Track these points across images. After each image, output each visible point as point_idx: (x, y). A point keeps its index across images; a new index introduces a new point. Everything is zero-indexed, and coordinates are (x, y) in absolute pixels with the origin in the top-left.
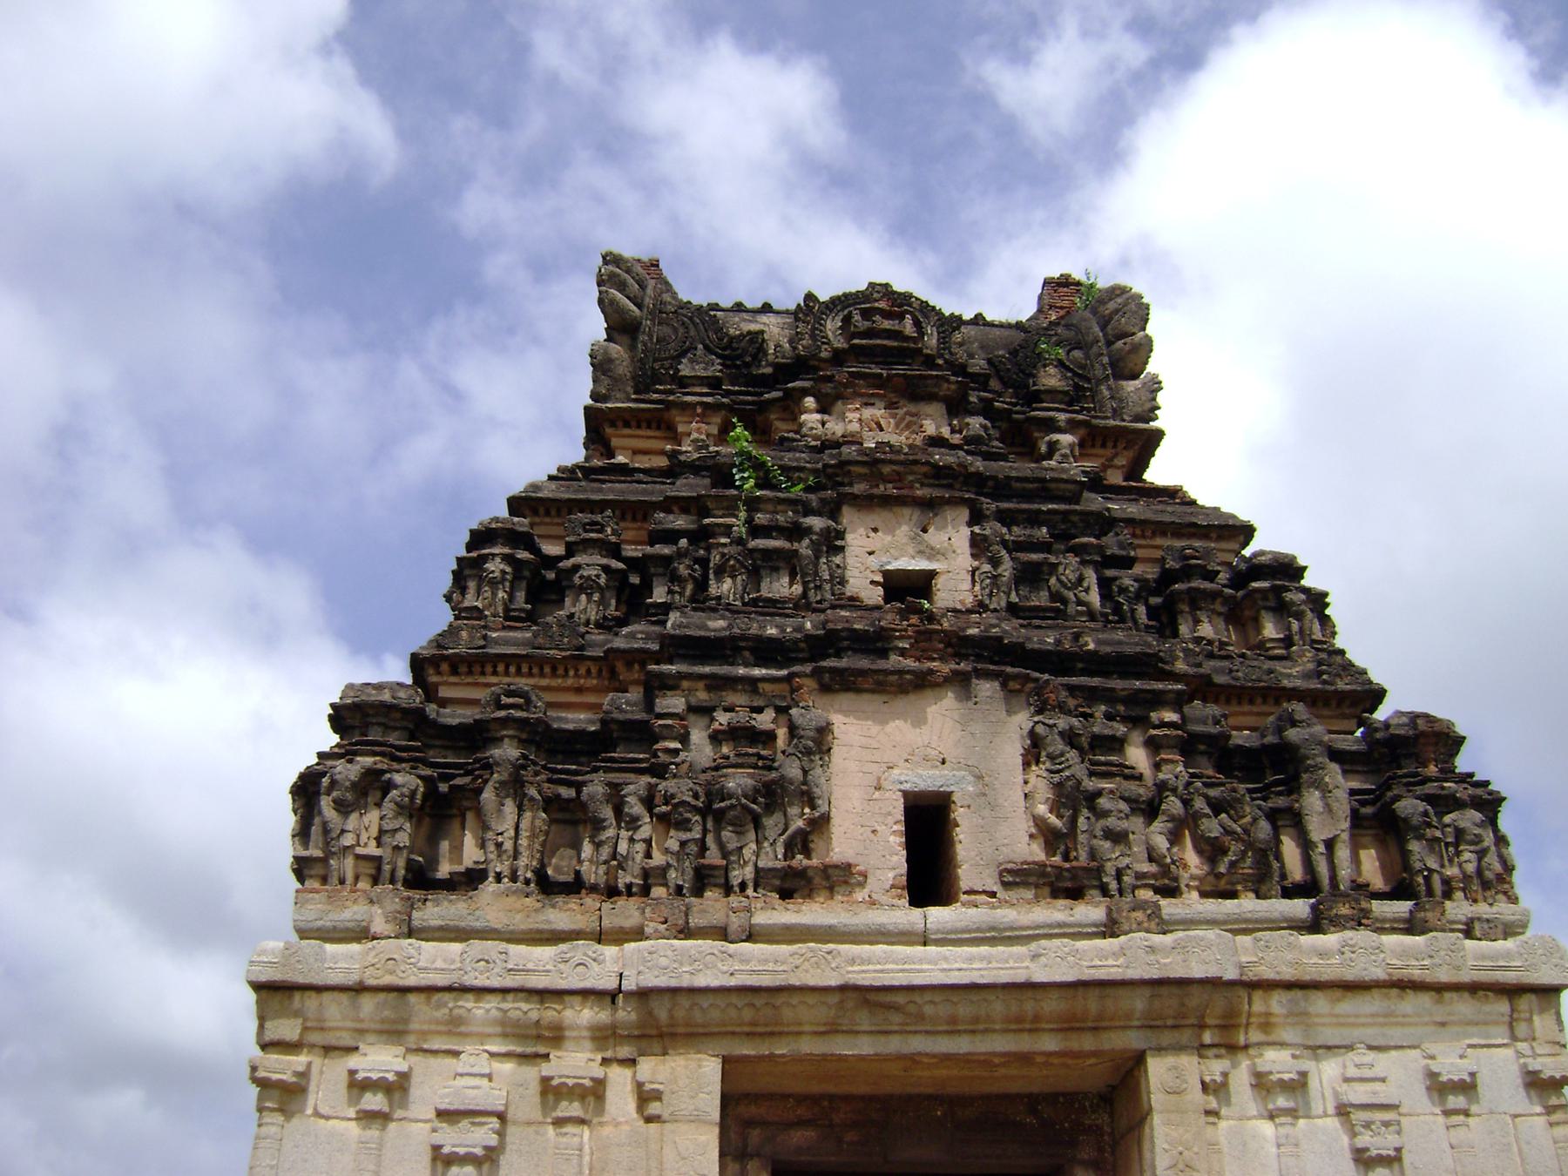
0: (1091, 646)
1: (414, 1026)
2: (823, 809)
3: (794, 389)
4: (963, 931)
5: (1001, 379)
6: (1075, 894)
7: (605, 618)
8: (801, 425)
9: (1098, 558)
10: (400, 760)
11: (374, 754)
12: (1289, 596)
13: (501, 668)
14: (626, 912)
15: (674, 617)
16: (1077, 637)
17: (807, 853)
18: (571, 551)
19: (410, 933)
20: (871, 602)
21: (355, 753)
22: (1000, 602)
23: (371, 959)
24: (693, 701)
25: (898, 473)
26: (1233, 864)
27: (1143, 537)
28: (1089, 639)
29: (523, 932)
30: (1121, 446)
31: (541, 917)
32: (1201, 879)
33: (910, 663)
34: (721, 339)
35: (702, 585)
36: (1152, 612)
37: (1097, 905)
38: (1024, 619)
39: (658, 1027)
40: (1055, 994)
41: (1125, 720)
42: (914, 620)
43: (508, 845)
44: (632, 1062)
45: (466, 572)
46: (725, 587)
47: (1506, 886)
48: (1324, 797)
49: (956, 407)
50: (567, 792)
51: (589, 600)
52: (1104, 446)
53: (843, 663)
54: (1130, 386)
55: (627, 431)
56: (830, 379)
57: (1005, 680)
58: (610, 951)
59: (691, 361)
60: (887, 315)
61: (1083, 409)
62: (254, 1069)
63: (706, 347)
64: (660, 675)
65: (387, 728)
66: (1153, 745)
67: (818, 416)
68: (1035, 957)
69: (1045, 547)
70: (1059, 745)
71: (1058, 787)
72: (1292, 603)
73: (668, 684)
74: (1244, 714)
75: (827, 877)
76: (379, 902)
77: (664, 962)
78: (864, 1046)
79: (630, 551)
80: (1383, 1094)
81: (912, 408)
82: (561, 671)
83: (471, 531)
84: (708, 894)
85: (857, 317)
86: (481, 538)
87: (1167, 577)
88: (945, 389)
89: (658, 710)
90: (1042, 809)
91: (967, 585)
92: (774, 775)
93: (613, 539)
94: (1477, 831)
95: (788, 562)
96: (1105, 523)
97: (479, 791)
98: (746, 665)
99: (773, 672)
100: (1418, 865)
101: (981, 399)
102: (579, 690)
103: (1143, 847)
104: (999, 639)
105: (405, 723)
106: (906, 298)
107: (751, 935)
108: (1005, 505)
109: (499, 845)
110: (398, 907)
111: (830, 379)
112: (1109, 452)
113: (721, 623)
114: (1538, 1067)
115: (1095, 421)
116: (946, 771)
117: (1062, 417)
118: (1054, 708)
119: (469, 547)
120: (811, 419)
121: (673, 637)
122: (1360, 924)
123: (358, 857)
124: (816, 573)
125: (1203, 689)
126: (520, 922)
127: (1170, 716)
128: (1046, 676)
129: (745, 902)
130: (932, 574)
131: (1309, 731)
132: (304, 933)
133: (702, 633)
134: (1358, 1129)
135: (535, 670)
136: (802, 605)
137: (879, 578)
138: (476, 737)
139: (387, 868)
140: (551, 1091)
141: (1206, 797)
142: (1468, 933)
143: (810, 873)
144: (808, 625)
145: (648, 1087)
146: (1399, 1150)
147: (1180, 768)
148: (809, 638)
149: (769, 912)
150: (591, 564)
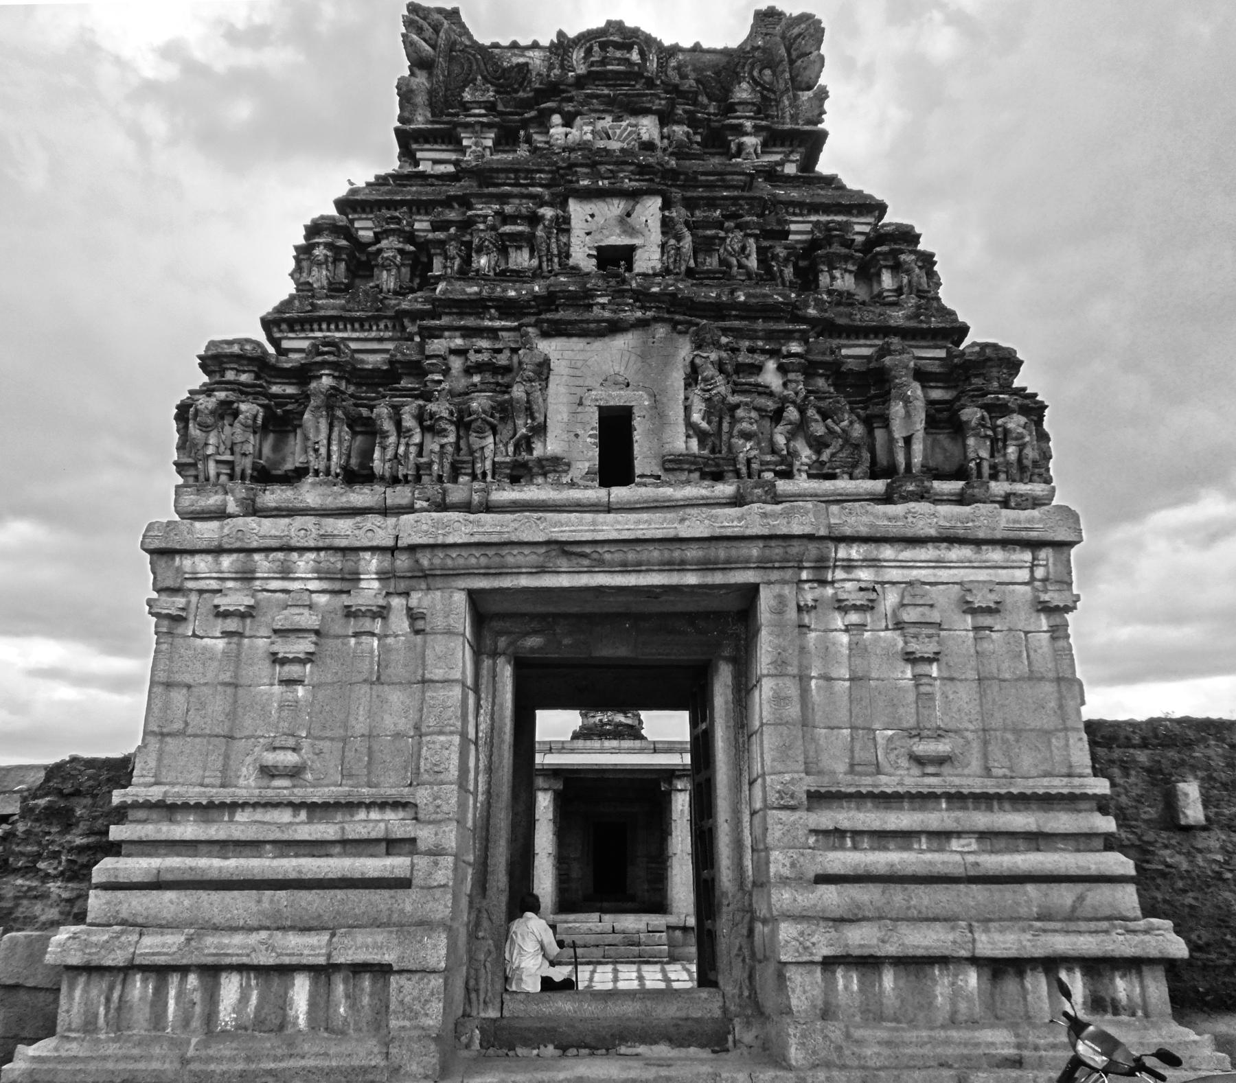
0: (742, 298)
3: (544, 109)
4: (636, 503)
6: (718, 477)
8: (551, 137)
9: (758, 232)
10: (247, 394)
11: (227, 390)
12: (903, 257)
13: (324, 326)
14: (399, 495)
15: (441, 286)
16: (732, 292)
17: (530, 450)
20: (587, 270)
21: (214, 390)
23: (226, 531)
24: (452, 346)
25: (611, 171)
26: (833, 455)
27: (801, 215)
30: (796, 143)
31: (344, 499)
32: (810, 466)
33: (607, 314)
35: (467, 261)
36: (798, 271)
39: (422, 570)
43: (323, 451)
44: (406, 594)
45: (304, 253)
47: (1043, 470)
48: (906, 406)
49: (665, 119)
50: (365, 412)
51: (389, 275)
52: (782, 145)
53: (561, 315)
54: (805, 96)
57: (674, 324)
58: (391, 521)
60: (618, 46)
63: (484, 78)
66: (782, 369)
68: (682, 520)
70: (710, 371)
72: (906, 262)
74: (860, 346)
75: (542, 467)
76: (232, 492)
77: (425, 527)
78: (564, 581)
81: (633, 120)
82: (367, 327)
84: (461, 479)
85: (596, 48)
86: (314, 230)
87: (813, 245)
88: (659, 104)
89: (427, 353)
91: (657, 255)
93: (407, 229)
94: (1020, 430)
95: (529, 241)
96: (765, 206)
97: (302, 414)
98: (491, 319)
99: (508, 324)
100: (972, 455)
101: (685, 111)
102: (381, 340)
105: (251, 368)
106: (636, 32)
107: (488, 508)
109: (316, 451)
110: (244, 495)
111: (571, 100)
113: (476, 289)
115: (776, 126)
117: (748, 124)
118: (708, 344)
119: (307, 238)
120: (557, 131)
121: (440, 300)
123: (218, 462)
124: (548, 249)
125: (828, 328)
126: (330, 502)
127: (795, 348)
128: (705, 321)
129: (483, 485)
130: (632, 249)
135: (349, 326)
136: (537, 274)
139: (238, 470)
143: (531, 464)
144: (537, 288)
145: (415, 611)
148: (536, 297)
150: (390, 245)
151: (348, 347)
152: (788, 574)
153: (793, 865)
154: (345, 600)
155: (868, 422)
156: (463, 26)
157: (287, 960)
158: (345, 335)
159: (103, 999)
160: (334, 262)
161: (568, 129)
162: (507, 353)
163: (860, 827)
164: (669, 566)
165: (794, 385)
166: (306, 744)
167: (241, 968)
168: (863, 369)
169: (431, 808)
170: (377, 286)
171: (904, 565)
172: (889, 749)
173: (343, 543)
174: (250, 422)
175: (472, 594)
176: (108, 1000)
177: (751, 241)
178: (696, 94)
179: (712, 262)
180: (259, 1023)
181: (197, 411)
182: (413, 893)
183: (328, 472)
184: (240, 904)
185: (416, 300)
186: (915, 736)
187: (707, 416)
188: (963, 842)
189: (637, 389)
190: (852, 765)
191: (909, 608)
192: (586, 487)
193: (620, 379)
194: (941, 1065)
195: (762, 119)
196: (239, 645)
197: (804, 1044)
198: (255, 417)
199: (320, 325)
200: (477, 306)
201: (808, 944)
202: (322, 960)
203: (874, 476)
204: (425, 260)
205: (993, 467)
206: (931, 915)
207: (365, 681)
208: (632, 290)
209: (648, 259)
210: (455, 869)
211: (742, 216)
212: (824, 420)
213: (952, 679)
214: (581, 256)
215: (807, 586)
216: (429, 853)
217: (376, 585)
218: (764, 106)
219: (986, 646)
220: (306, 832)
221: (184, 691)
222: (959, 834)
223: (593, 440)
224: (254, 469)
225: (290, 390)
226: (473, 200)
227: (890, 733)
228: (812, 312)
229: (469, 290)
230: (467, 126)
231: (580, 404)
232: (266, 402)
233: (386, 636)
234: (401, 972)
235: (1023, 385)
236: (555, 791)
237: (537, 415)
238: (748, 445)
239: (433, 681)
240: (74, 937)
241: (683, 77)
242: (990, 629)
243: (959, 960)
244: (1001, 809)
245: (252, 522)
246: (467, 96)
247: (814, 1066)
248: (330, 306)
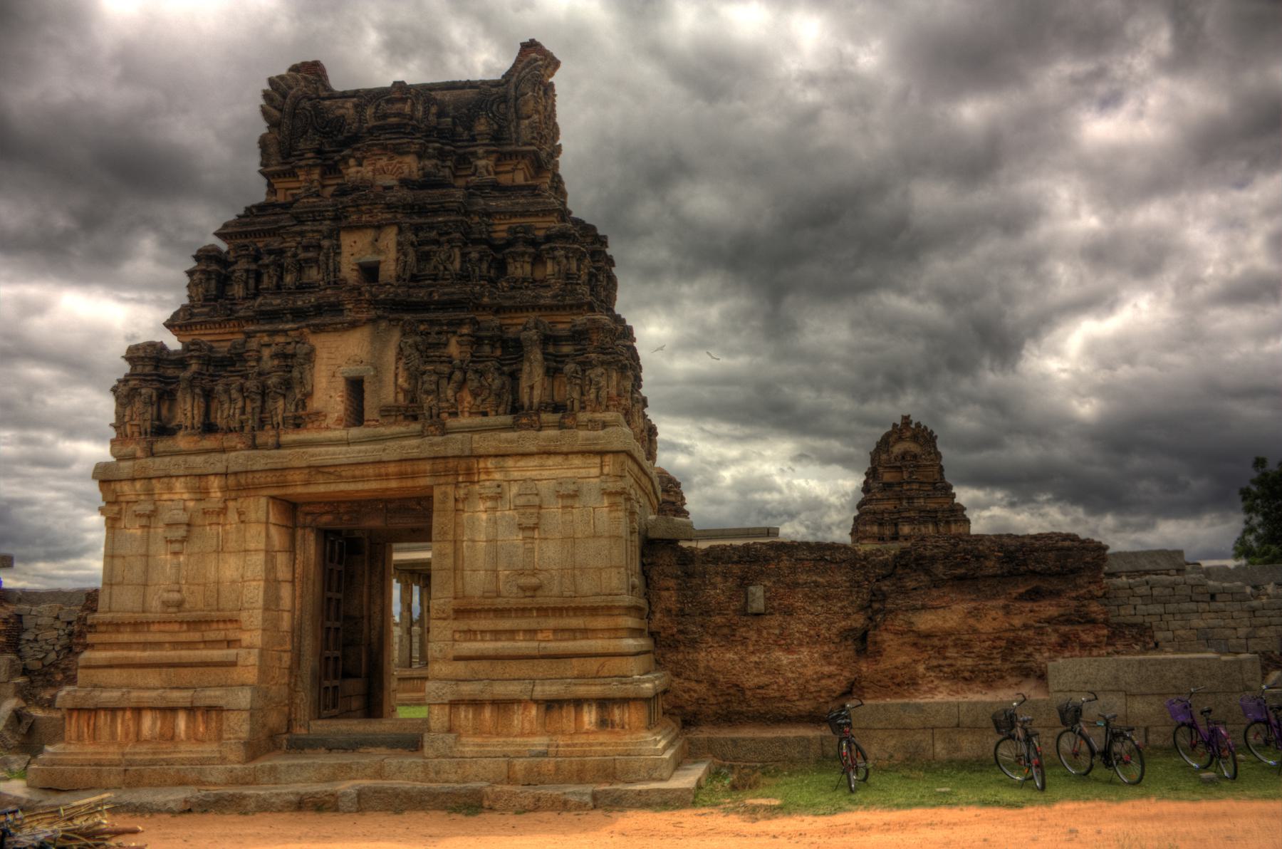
0: (436, 298)
1: (156, 491)
2: (309, 388)
17: (304, 407)
24: (262, 342)
30: (520, 158)
40: (393, 465)
43: (189, 414)
58: (225, 456)
78: (322, 489)
81: (400, 159)
85: (383, 104)
102: (232, 333)
111: (358, 149)
112: (515, 162)
117: (480, 151)
126: (192, 446)
130: (379, 262)
137: (355, 267)
144: (313, 300)
152: (450, 479)
153: (441, 651)
154: (203, 505)
161: (359, 168)
162: (293, 344)
163: (485, 628)
164: (379, 477)
166: (184, 588)
167: (152, 709)
169: (248, 623)
171: (521, 469)
173: (199, 472)
176: (88, 725)
179: (429, 269)
180: (162, 736)
182: (239, 669)
183: (193, 428)
184: (153, 678)
188: (544, 635)
192: (335, 429)
193: (357, 358)
196: (148, 532)
198: (151, 397)
202: (188, 705)
205: (582, 402)
209: (389, 269)
211: (450, 233)
213: (546, 539)
214: (348, 271)
215: (463, 485)
217: (219, 494)
220: (183, 637)
221: (121, 560)
222: (541, 631)
224: (152, 427)
227: (507, 572)
230: (300, 167)
231: (334, 376)
234: (228, 710)
238: (430, 398)
240: (68, 693)
242: (572, 507)
243: (526, 702)
244: (568, 616)
245: (150, 461)
246: (302, 146)
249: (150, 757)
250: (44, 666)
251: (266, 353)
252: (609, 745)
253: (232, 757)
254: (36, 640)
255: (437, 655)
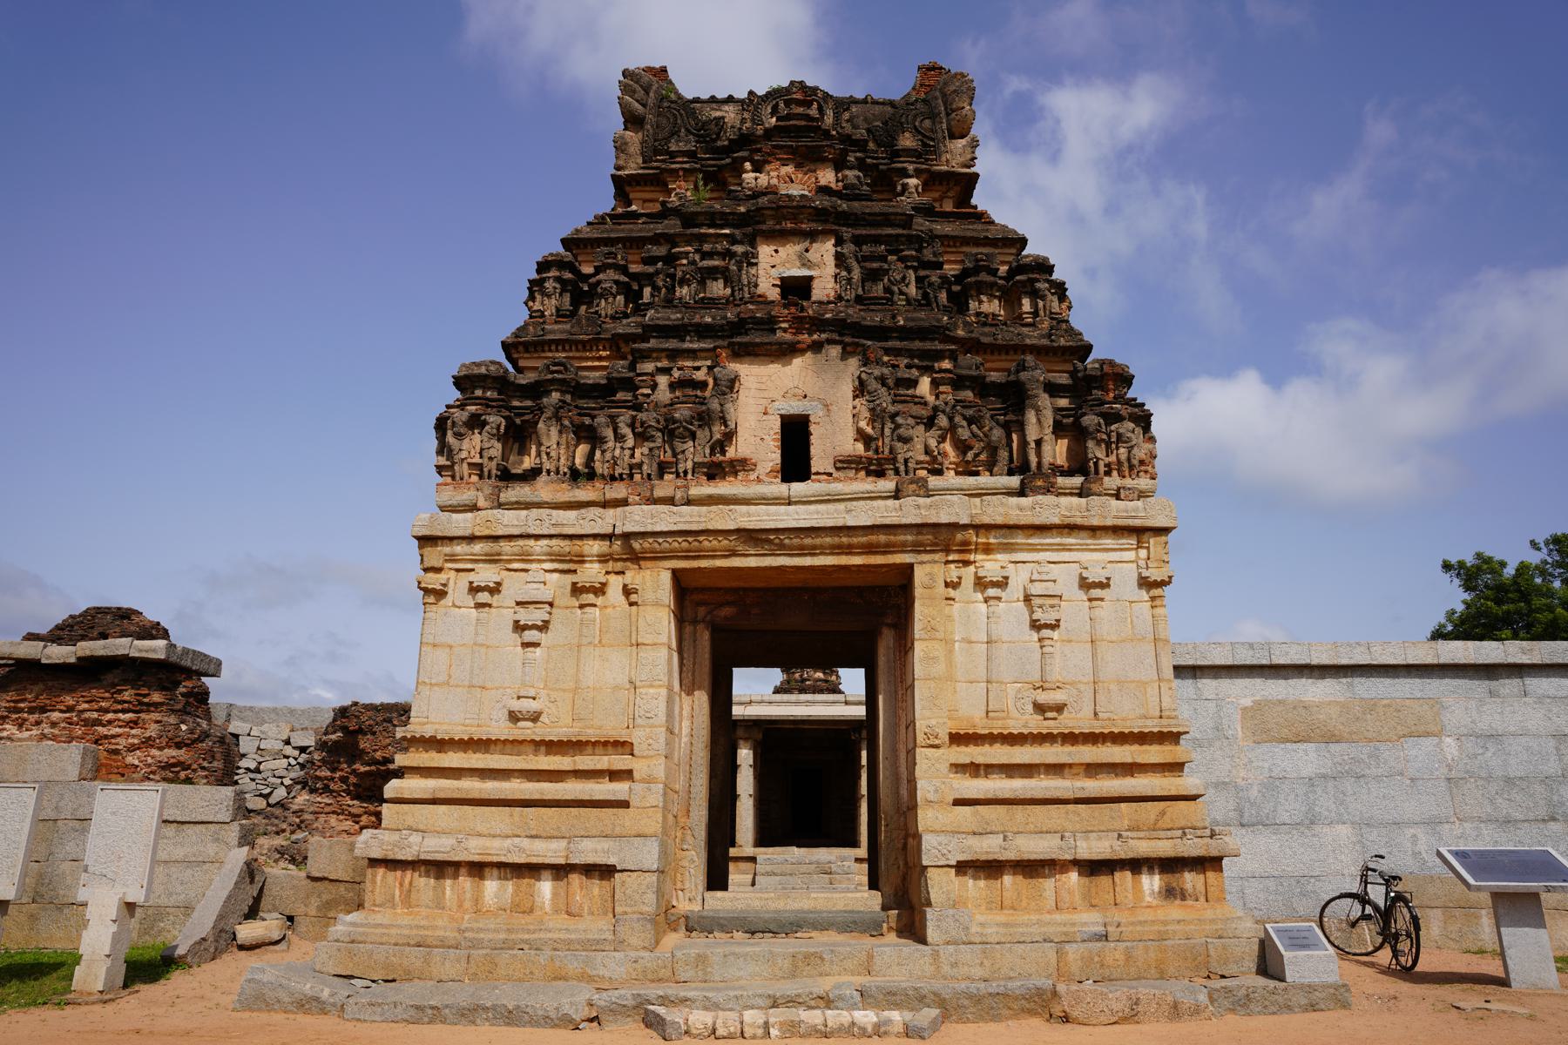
0: (902, 323)
5: (875, 141)
6: (880, 474)
7: (616, 313)
8: (743, 181)
9: (916, 264)
10: (493, 407)
11: (476, 405)
12: (1038, 285)
13: (553, 348)
14: (618, 491)
15: (651, 313)
16: (894, 317)
17: (723, 452)
18: (598, 270)
19: (500, 506)
21: (466, 405)
22: (850, 295)
24: (659, 365)
26: (977, 455)
27: (955, 246)
28: (900, 318)
29: (562, 503)
30: (952, 184)
33: (788, 337)
34: (697, 124)
35: (672, 290)
36: (950, 295)
37: (892, 480)
38: (865, 305)
41: (918, 368)
42: (793, 310)
45: (536, 287)
46: (683, 292)
49: (839, 165)
50: (587, 421)
52: (941, 184)
55: (638, 188)
56: (759, 150)
58: (611, 512)
59: (677, 141)
60: (799, 103)
61: (927, 160)
62: (419, 583)
63: (687, 130)
64: (639, 350)
65: (485, 389)
66: (935, 384)
67: (753, 175)
69: (884, 259)
70: (873, 385)
71: (872, 410)
72: (1040, 290)
73: (646, 355)
74: (1001, 361)
77: (637, 518)
78: (752, 562)
79: (635, 268)
80: (1051, 589)
82: (588, 348)
83: (537, 263)
84: (666, 477)
85: (782, 105)
86: (543, 266)
87: (965, 273)
90: (863, 424)
92: (704, 408)
96: (918, 241)
97: (537, 423)
100: (1090, 456)
101: (856, 158)
102: (600, 358)
103: (923, 446)
104: (844, 320)
105: (495, 385)
106: (815, 89)
108: (858, 232)
111: (759, 150)
112: (944, 188)
114: (1147, 575)
116: (806, 402)
117: (911, 167)
119: (539, 271)
120: (749, 177)
121: (649, 326)
122: (1049, 491)
123: (469, 464)
124: (740, 281)
125: (973, 346)
127: (946, 364)
128: (869, 343)
130: (811, 278)
131: (1037, 374)
132: (443, 508)
133: (667, 323)
134: (1035, 609)
136: (730, 302)
138: (536, 391)
139: (486, 470)
140: (577, 590)
141: (963, 415)
142: (1118, 497)
144: (729, 315)
145: (630, 587)
146: (1058, 621)
147: (950, 397)
148: (730, 323)
149: (699, 488)
151: (572, 366)
153: (936, 791)
155: (1007, 428)
156: (671, 82)
157: (534, 860)
158: (571, 354)
159: (397, 884)
160: (561, 295)
165: (944, 396)
166: (543, 693)
168: (1004, 381)
170: (596, 312)
172: (1017, 699)
174: (495, 431)
175: (675, 572)
177: (911, 272)
178: (866, 142)
181: (454, 422)
185: (628, 325)
186: (1038, 688)
187: (872, 421)
189: (812, 399)
190: (987, 712)
191: (1036, 583)
194: (1045, 940)
195: (923, 163)
197: (938, 926)
198: (499, 427)
199: (550, 347)
200: (678, 331)
201: (945, 851)
202: (562, 861)
203: (1011, 473)
204: (636, 288)
206: (1045, 829)
207: (590, 643)
208: (809, 317)
209: (825, 288)
210: (665, 794)
211: (903, 250)
212: (969, 425)
215: (952, 566)
216: (643, 781)
218: (928, 150)
219: (1097, 612)
221: (447, 650)
223: (776, 444)
225: (529, 403)
226: (677, 240)
228: (960, 333)
229: (673, 317)
232: (507, 413)
233: (605, 607)
235: (1134, 396)
236: (755, 741)
237: (729, 423)
239: (644, 644)
241: (855, 127)
247: (948, 943)
248: (557, 330)
249: (502, 936)
250: (269, 805)
251: (663, 380)
252: (1190, 923)
253: (634, 941)
254: (257, 771)
255: (931, 797)
